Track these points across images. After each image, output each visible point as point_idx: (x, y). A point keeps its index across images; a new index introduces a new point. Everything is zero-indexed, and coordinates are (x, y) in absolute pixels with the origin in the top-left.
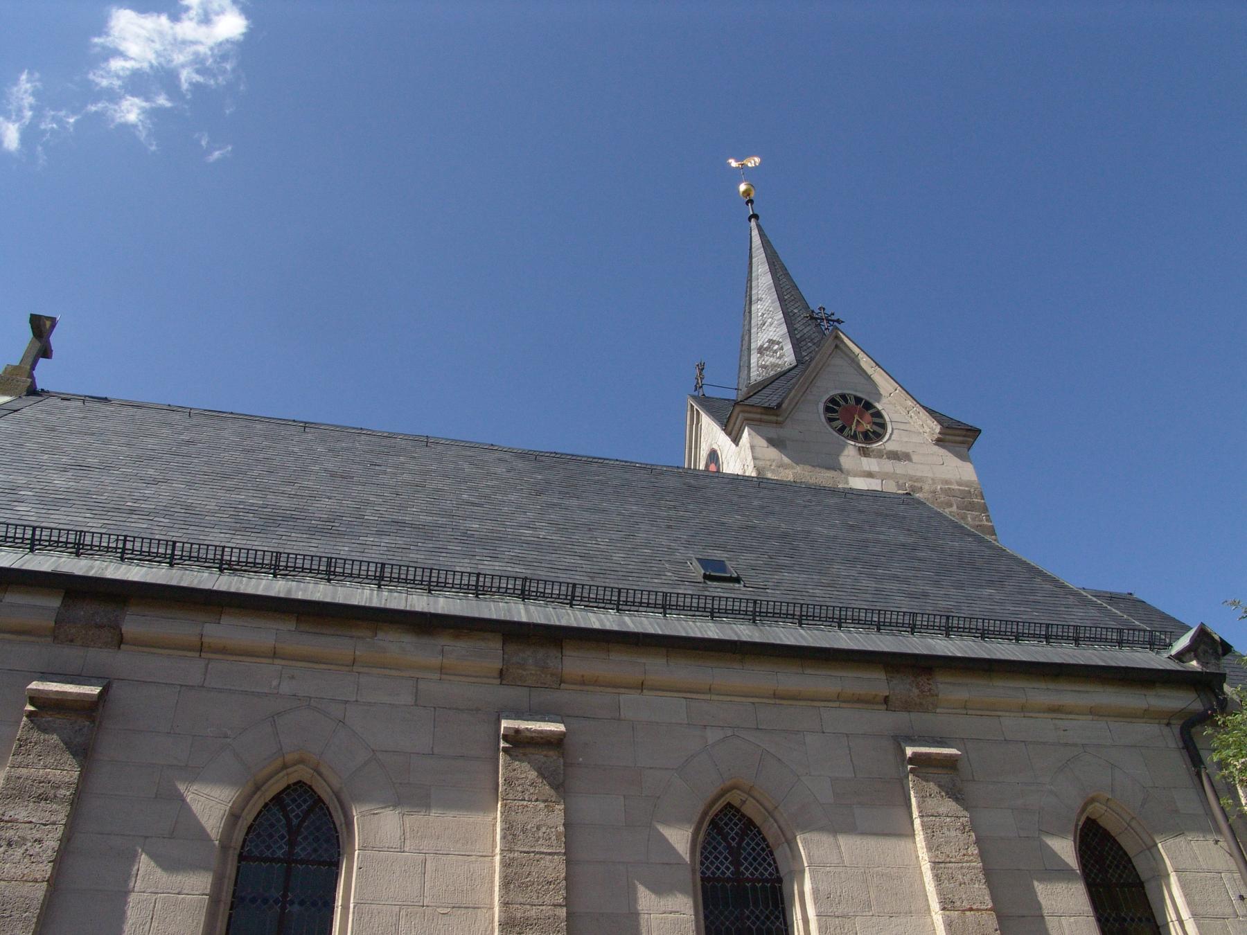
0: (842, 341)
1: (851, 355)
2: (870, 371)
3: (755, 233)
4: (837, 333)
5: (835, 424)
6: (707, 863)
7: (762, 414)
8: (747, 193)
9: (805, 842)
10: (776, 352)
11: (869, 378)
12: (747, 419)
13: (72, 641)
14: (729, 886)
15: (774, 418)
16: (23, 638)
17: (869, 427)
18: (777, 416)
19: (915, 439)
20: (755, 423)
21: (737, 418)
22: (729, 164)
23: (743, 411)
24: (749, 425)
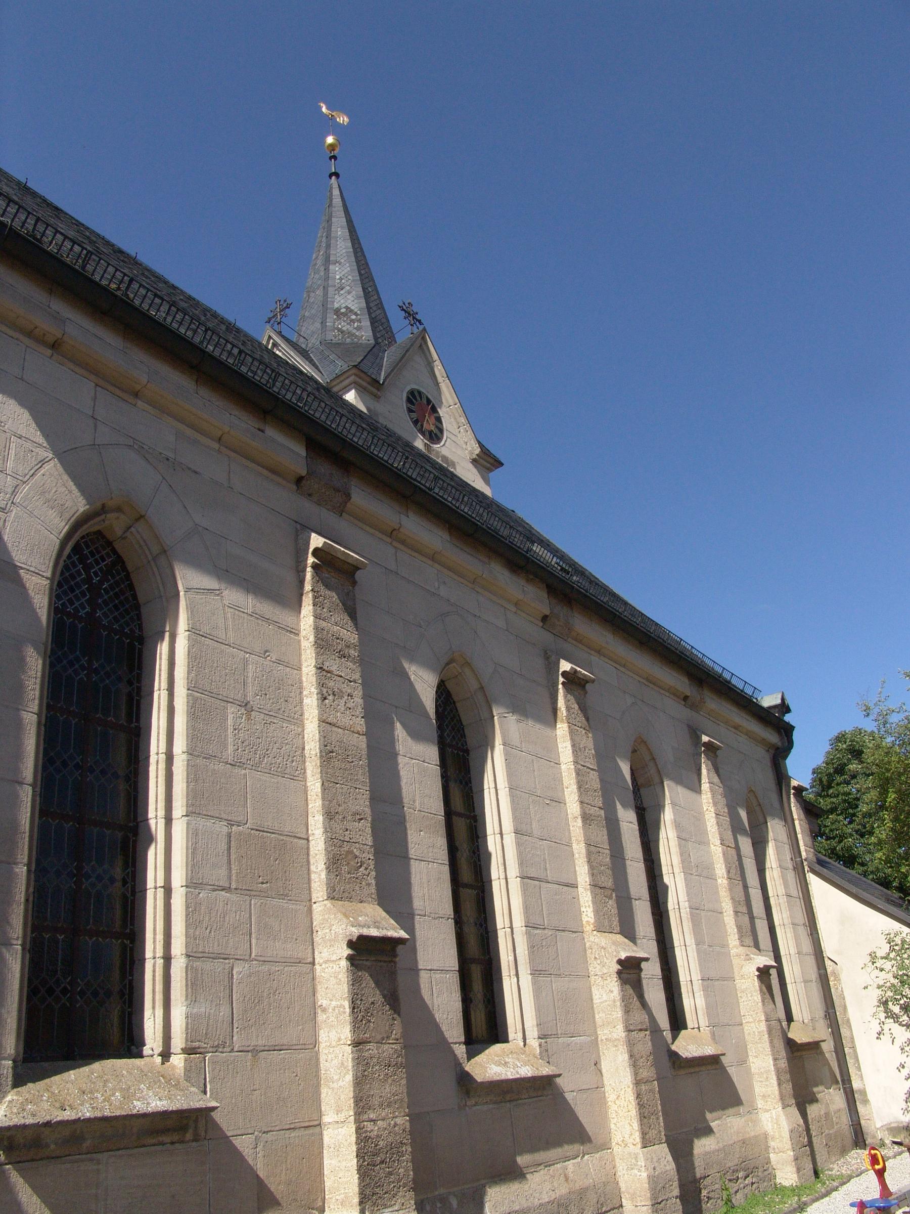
0: (426, 343)
1: (430, 360)
2: (440, 379)
3: (336, 192)
4: (424, 334)
5: (414, 415)
6: (65, 599)
7: (369, 383)
8: (332, 147)
9: (668, 785)
10: (353, 321)
11: (437, 384)
12: (355, 383)
13: (310, 495)
14: (80, 626)
15: (375, 391)
16: (274, 477)
17: (433, 429)
18: (378, 390)
19: (459, 452)
20: (361, 389)
21: (348, 377)
22: (321, 108)
23: (355, 375)
24: (356, 390)
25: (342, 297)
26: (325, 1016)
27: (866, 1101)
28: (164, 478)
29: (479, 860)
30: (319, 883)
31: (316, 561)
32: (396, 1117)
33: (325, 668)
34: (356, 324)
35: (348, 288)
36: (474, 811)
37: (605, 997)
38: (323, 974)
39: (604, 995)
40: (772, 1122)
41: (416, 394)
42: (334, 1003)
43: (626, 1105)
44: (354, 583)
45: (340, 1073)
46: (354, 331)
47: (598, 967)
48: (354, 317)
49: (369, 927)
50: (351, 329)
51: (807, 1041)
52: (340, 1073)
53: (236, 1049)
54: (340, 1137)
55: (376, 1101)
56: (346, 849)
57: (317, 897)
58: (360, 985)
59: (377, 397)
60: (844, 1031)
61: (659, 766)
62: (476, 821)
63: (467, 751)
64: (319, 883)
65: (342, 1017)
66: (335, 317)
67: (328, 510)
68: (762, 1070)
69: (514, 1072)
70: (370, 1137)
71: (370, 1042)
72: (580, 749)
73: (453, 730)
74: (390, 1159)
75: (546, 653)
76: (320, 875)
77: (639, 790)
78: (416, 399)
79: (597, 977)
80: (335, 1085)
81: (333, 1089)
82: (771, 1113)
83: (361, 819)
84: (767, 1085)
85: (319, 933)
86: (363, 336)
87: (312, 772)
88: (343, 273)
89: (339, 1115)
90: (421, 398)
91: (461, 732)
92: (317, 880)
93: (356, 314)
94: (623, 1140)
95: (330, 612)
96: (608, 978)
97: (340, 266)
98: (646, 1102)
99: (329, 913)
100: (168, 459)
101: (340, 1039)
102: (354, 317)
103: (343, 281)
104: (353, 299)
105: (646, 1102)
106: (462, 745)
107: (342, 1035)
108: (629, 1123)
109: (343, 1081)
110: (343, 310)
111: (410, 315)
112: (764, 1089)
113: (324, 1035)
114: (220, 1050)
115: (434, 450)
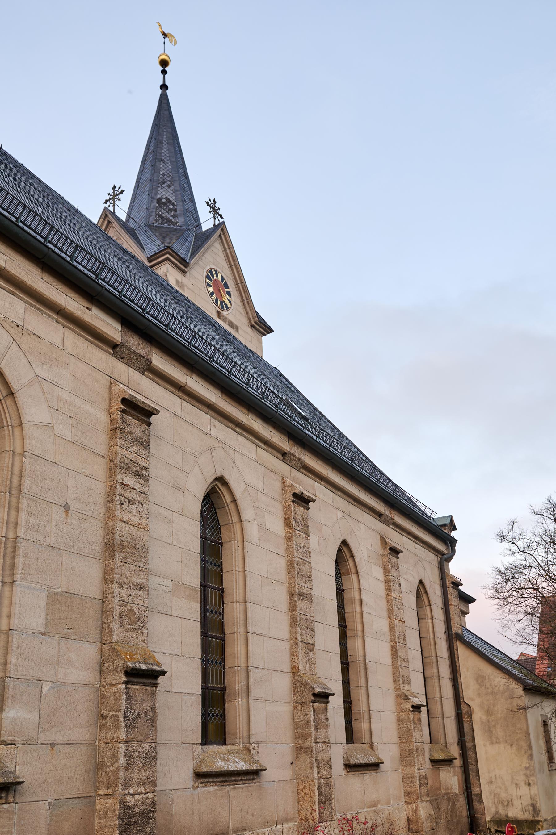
10: (171, 210)
13: (122, 358)
18: (186, 267)
25: (164, 189)
26: (104, 722)
27: (481, 801)
28: (14, 340)
29: (223, 619)
30: (108, 631)
31: (123, 407)
32: (147, 793)
33: (124, 483)
34: (173, 212)
35: (169, 183)
36: (222, 585)
37: (302, 718)
38: (105, 693)
39: (301, 717)
40: (412, 811)
41: (214, 272)
42: (111, 713)
43: (309, 793)
44: (149, 424)
45: (112, 762)
46: (171, 218)
47: (299, 697)
48: (171, 207)
49: (140, 663)
50: (168, 216)
51: (444, 758)
52: (112, 762)
53: (39, 742)
54: (108, 805)
55: (134, 782)
56: (129, 608)
57: (106, 640)
58: (131, 702)
59: (184, 272)
60: (471, 754)
61: (356, 562)
62: (223, 592)
63: (221, 544)
64: (108, 631)
65: (116, 723)
66: (157, 205)
67: (135, 369)
68: (409, 776)
69: (233, 766)
70: (128, 806)
71: (134, 741)
72: (300, 547)
73: (213, 528)
74: (141, 821)
75: (283, 479)
76: (109, 625)
77: (341, 576)
78: (213, 277)
79: (298, 704)
80: (107, 769)
81: (106, 772)
82: (412, 805)
83: (142, 588)
84: (411, 786)
85: (105, 665)
86: (177, 222)
87: (109, 554)
88: (166, 170)
89: (109, 790)
90: (217, 276)
91: (219, 530)
92: (107, 629)
93: (173, 205)
94: (306, 817)
95: (131, 443)
96: (305, 705)
97: (163, 164)
98: (323, 792)
99: (113, 652)
100: (18, 326)
101: (113, 738)
102: (171, 207)
103: (165, 177)
104: (172, 192)
105: (323, 792)
106: (218, 539)
107: (115, 736)
108: (311, 806)
109: (113, 767)
110: (164, 200)
111: (214, 210)
112: (409, 789)
113: (102, 735)
114: (29, 743)
115: (223, 316)
